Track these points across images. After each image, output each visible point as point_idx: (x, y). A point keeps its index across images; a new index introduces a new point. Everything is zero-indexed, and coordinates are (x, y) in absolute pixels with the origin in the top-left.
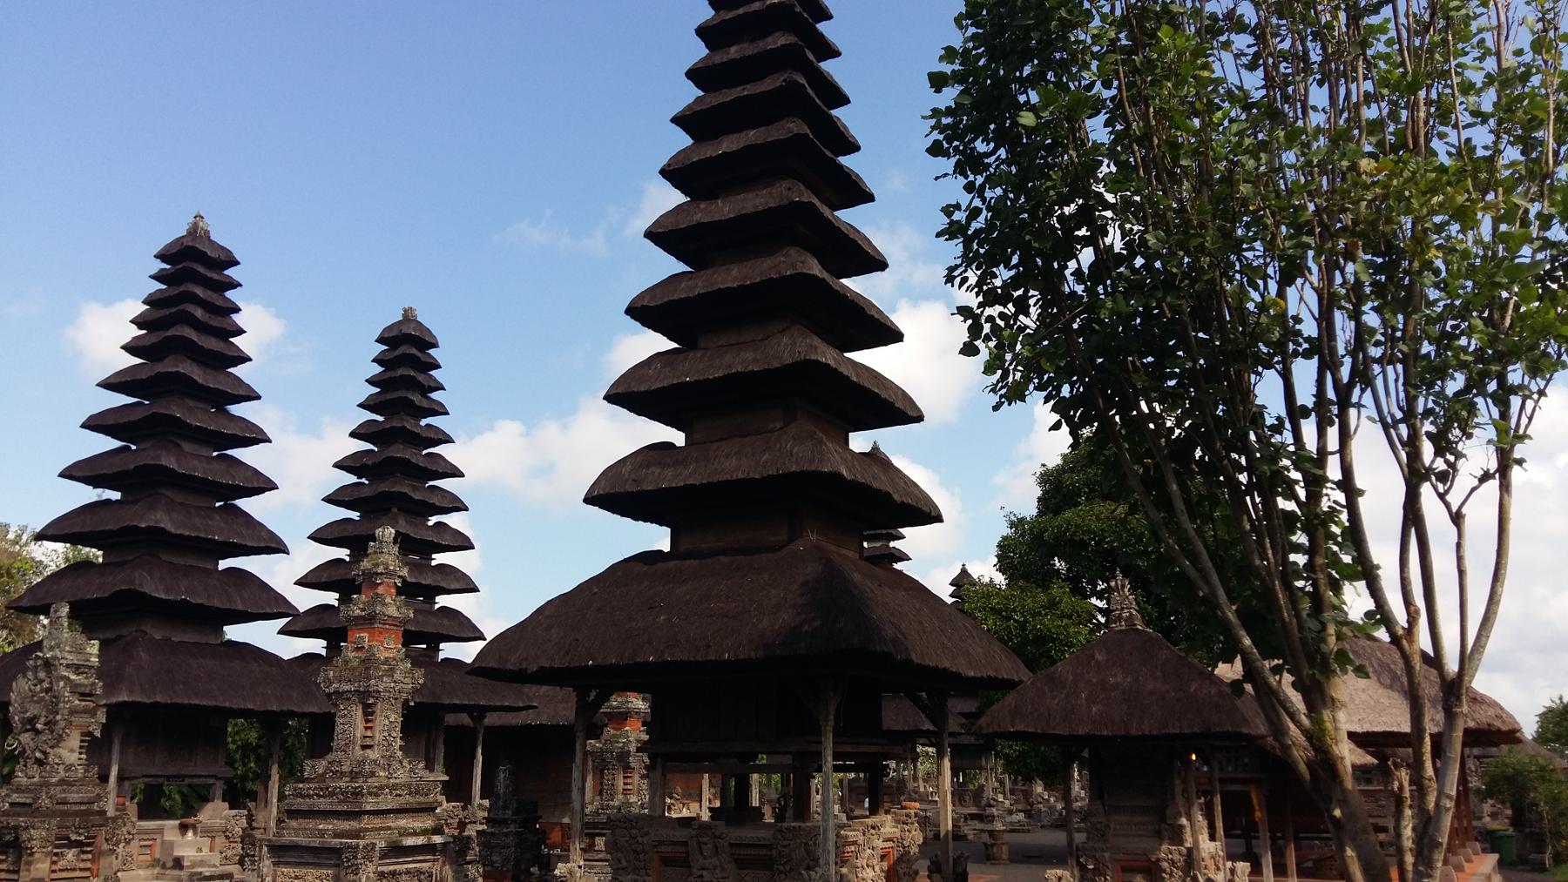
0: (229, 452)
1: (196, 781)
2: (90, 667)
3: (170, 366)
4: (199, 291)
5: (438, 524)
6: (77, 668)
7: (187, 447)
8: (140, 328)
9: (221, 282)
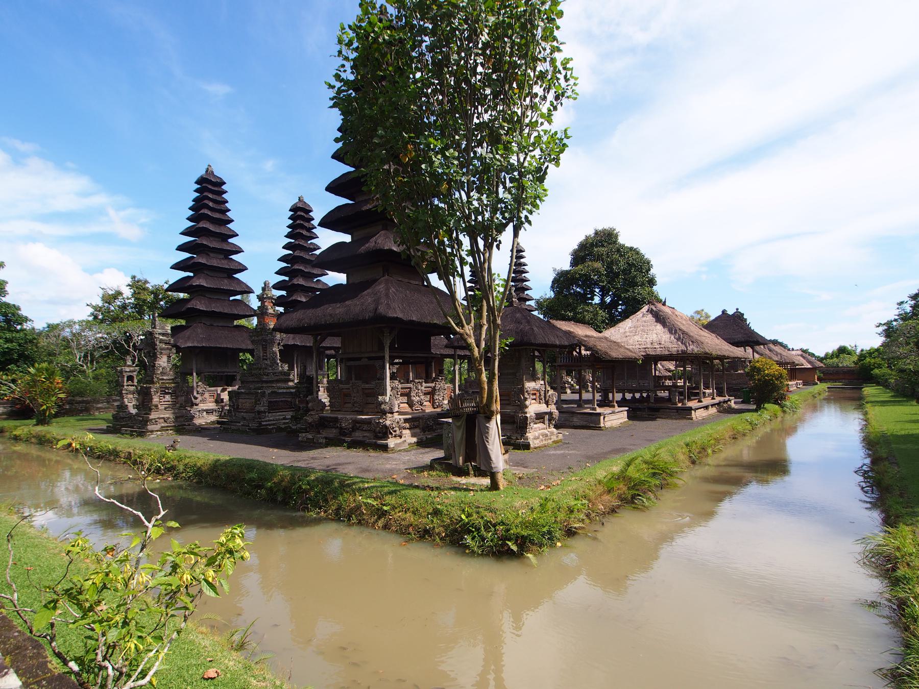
0: (314, 253)
1: (229, 374)
2: (168, 334)
3: (203, 224)
4: (210, 196)
5: (318, 280)
6: (163, 334)
7: (212, 255)
8: (193, 211)
9: (219, 191)
